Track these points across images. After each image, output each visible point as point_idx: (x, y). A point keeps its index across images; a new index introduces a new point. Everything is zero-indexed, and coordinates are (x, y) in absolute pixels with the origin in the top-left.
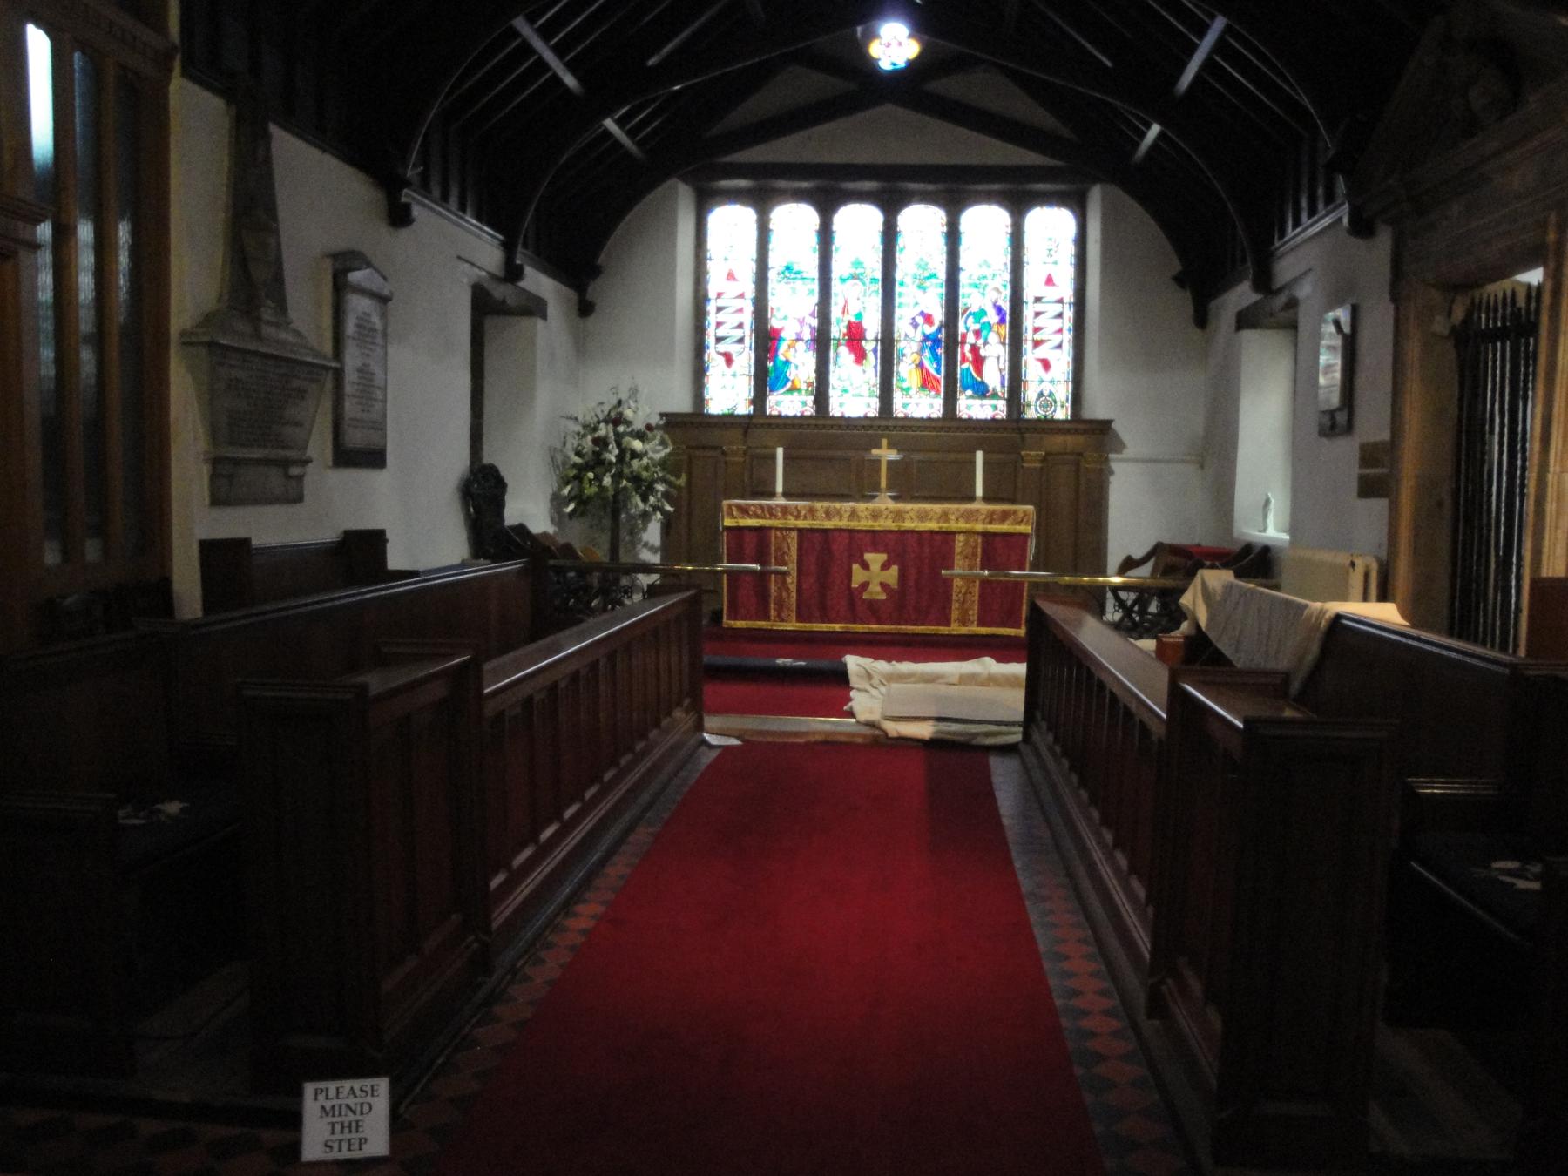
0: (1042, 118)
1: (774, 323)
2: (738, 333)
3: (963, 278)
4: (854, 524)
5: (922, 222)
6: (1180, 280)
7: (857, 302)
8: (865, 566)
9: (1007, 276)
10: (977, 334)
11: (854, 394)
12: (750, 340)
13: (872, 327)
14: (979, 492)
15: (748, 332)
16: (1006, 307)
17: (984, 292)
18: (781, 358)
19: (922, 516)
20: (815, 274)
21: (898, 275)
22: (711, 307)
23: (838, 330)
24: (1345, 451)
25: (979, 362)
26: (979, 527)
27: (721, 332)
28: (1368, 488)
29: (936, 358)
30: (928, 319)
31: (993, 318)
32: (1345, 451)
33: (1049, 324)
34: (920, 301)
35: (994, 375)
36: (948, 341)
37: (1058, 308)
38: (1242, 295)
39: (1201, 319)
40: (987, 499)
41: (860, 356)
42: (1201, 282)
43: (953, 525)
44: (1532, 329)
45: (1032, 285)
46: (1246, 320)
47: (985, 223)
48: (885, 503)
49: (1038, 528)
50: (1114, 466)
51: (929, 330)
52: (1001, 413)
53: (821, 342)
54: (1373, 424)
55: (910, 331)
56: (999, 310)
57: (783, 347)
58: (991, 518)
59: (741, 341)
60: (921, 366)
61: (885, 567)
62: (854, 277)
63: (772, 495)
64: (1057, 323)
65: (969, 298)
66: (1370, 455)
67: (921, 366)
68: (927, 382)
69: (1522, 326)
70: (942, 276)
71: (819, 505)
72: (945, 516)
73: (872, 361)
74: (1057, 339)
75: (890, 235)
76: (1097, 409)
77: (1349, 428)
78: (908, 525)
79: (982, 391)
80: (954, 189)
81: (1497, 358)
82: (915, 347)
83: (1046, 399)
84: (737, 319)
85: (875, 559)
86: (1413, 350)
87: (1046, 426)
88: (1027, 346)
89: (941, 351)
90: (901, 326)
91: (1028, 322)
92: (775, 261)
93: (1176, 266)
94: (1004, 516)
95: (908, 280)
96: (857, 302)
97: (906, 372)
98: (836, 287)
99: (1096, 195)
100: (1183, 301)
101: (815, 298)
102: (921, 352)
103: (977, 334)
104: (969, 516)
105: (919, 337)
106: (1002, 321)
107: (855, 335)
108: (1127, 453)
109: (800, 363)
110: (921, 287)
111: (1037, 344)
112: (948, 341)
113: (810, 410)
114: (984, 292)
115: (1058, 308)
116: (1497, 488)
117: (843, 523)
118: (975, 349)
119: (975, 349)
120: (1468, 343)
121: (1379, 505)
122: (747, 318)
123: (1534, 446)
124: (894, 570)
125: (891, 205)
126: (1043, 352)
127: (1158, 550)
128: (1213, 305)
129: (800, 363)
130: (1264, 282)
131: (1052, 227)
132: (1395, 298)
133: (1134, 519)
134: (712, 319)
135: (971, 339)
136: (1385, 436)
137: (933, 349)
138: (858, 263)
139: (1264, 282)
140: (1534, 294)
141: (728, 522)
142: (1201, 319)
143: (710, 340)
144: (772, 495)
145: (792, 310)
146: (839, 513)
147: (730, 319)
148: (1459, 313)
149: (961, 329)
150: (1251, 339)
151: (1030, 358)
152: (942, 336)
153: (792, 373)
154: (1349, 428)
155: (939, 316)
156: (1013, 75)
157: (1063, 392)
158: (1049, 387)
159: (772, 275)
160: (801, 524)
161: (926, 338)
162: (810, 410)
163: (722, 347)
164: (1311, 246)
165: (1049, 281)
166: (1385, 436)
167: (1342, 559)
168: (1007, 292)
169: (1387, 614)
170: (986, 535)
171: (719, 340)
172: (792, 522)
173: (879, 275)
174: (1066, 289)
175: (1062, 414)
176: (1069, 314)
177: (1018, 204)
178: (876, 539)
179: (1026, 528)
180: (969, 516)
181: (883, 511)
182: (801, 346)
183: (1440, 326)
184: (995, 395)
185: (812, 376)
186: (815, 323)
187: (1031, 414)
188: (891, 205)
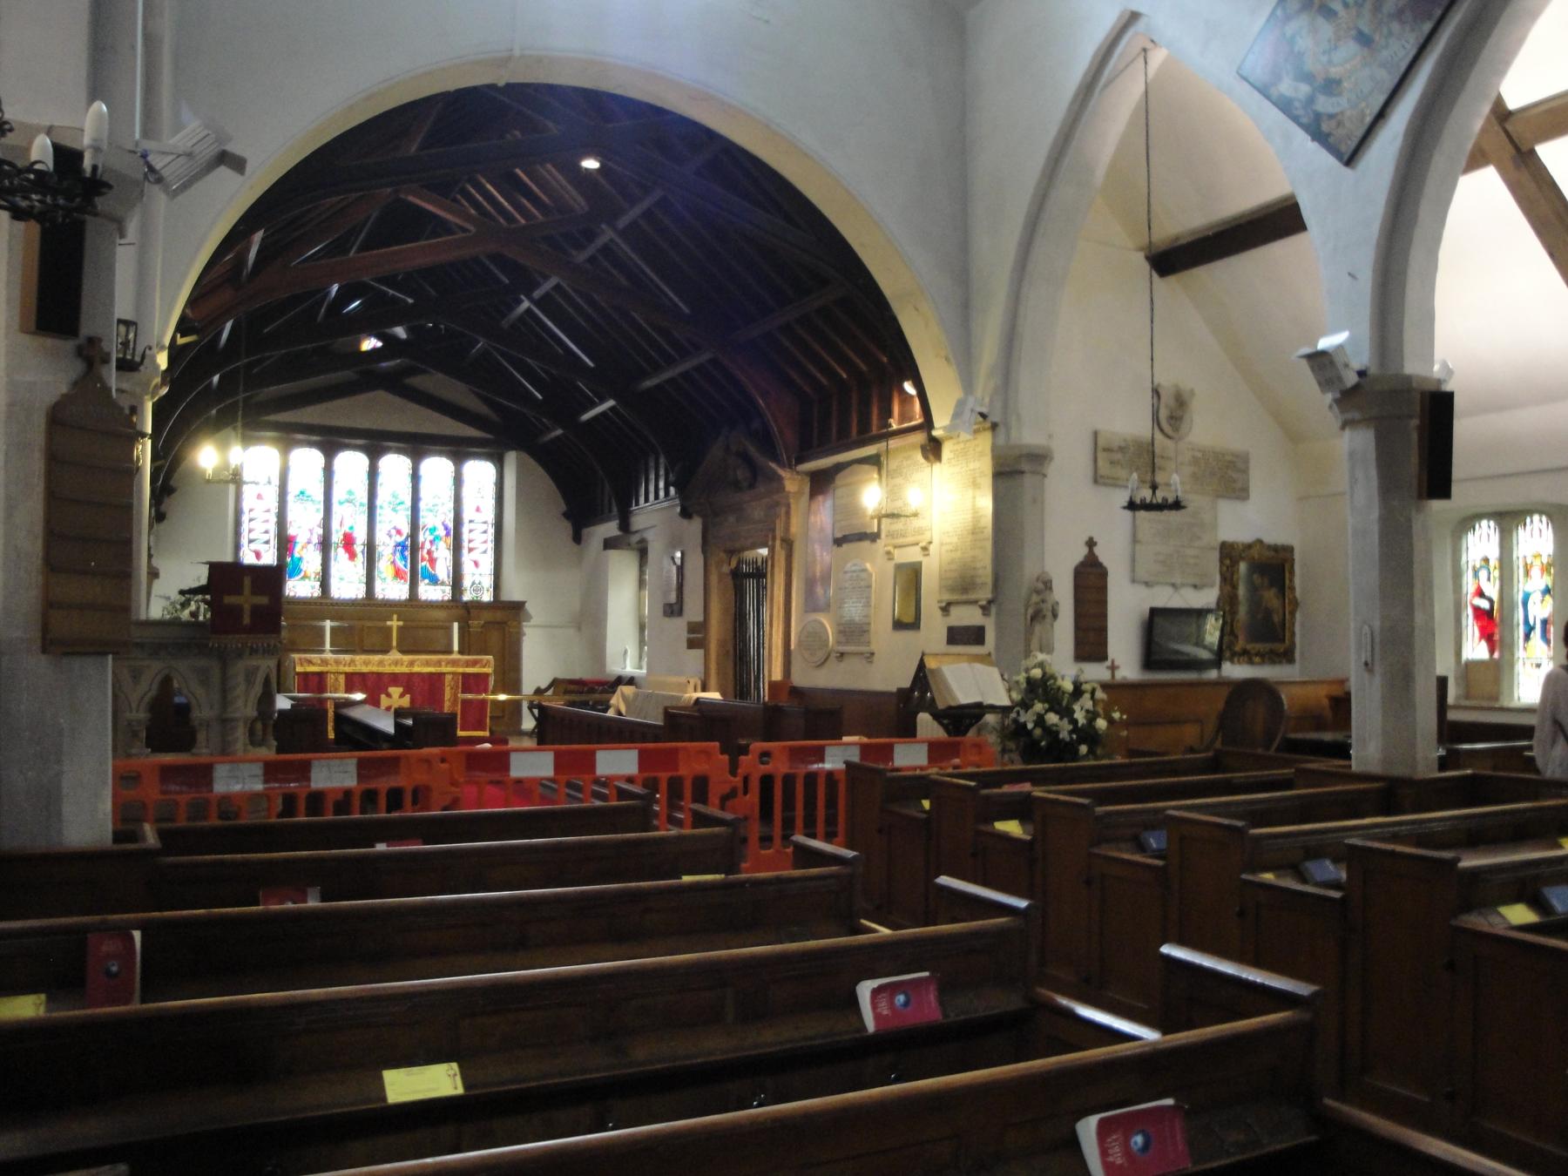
0: (484, 409)
1: (291, 531)
2: (266, 537)
3: (422, 505)
4: (381, 670)
5: (395, 465)
6: (567, 515)
7: (350, 518)
8: (389, 695)
9: (451, 505)
10: (432, 542)
11: (348, 583)
12: (274, 542)
13: (361, 537)
14: (456, 648)
15: (272, 536)
16: (451, 525)
17: (436, 515)
18: (296, 555)
19: (422, 665)
20: (321, 498)
21: (379, 502)
22: (245, 518)
23: (337, 537)
24: (678, 627)
25: (432, 561)
26: (461, 670)
27: (252, 536)
28: (692, 644)
29: (404, 558)
30: (399, 532)
31: (442, 532)
32: (678, 627)
33: (478, 538)
34: (392, 521)
35: (443, 570)
36: (412, 547)
37: (484, 527)
38: (610, 528)
39: (577, 538)
40: (461, 652)
41: (352, 556)
42: (580, 516)
43: (444, 669)
44: (764, 576)
45: (468, 514)
46: (609, 544)
47: (437, 468)
48: (395, 655)
49: (495, 671)
50: (526, 630)
51: (400, 539)
52: (448, 596)
53: (325, 545)
54: (693, 611)
55: (387, 539)
56: (446, 528)
57: (298, 548)
58: (468, 664)
59: (267, 542)
60: (393, 562)
61: (402, 696)
62: (349, 501)
63: (450, 652)
64: (484, 537)
65: (426, 519)
66: (693, 628)
67: (393, 562)
68: (398, 574)
69: (760, 573)
70: (409, 503)
71: (358, 657)
72: (412, 663)
73: (361, 559)
74: (483, 547)
75: (373, 474)
76: (513, 593)
77: (680, 613)
78: (416, 669)
79: (434, 581)
80: (417, 446)
81: (750, 585)
82: (390, 549)
83: (477, 587)
84: (265, 527)
85: (395, 691)
86: (714, 579)
87: (477, 605)
88: (465, 551)
89: (408, 553)
90: (380, 537)
91: (466, 536)
92: (293, 488)
93: (563, 507)
94: (475, 663)
95: (385, 505)
96: (350, 518)
97: (384, 567)
98: (336, 508)
99: (511, 458)
100: (566, 528)
101: (321, 515)
102: (394, 553)
103: (432, 542)
104: (454, 663)
105: (392, 544)
106: (448, 534)
107: (348, 542)
108: (532, 622)
109: (310, 560)
110: (394, 510)
111: (470, 550)
112: (412, 547)
113: (317, 593)
114: (436, 515)
115: (484, 527)
116: (753, 645)
117: (375, 669)
118: (429, 552)
119: (429, 552)
120: (738, 576)
121: (700, 652)
122: (272, 527)
123: (767, 628)
124: (407, 697)
125: (374, 454)
126: (474, 555)
127: (555, 683)
128: (585, 531)
129: (310, 560)
130: (625, 526)
131: (480, 473)
132: (704, 551)
133: (540, 664)
134: (245, 527)
135: (427, 546)
136: (701, 619)
137: (402, 553)
138: (350, 493)
139: (625, 526)
140: (765, 561)
141: (299, 669)
142: (577, 538)
143: (244, 541)
144: (450, 652)
145: (304, 523)
146: (310, 662)
147: (259, 527)
148: (734, 564)
149: (421, 539)
150: (614, 555)
151: (466, 559)
152: (408, 543)
153: (303, 566)
154: (680, 613)
155: (406, 530)
156: (477, 394)
157: (488, 582)
158: (479, 582)
159: (290, 498)
160: (347, 669)
161: (398, 545)
162: (317, 593)
163: (254, 546)
164: (655, 510)
165: (478, 510)
166: (701, 619)
167: (683, 680)
168: (452, 515)
169: (715, 695)
170: (464, 675)
171: (251, 541)
172: (342, 669)
173: (365, 501)
174: (489, 515)
175: (487, 597)
176: (491, 531)
177: (459, 457)
178: (395, 679)
179: (489, 670)
180: (454, 663)
181: (394, 662)
182: (311, 547)
183: (726, 569)
184: (443, 583)
185: (319, 568)
186: (321, 531)
187: (467, 597)
188: (374, 454)
